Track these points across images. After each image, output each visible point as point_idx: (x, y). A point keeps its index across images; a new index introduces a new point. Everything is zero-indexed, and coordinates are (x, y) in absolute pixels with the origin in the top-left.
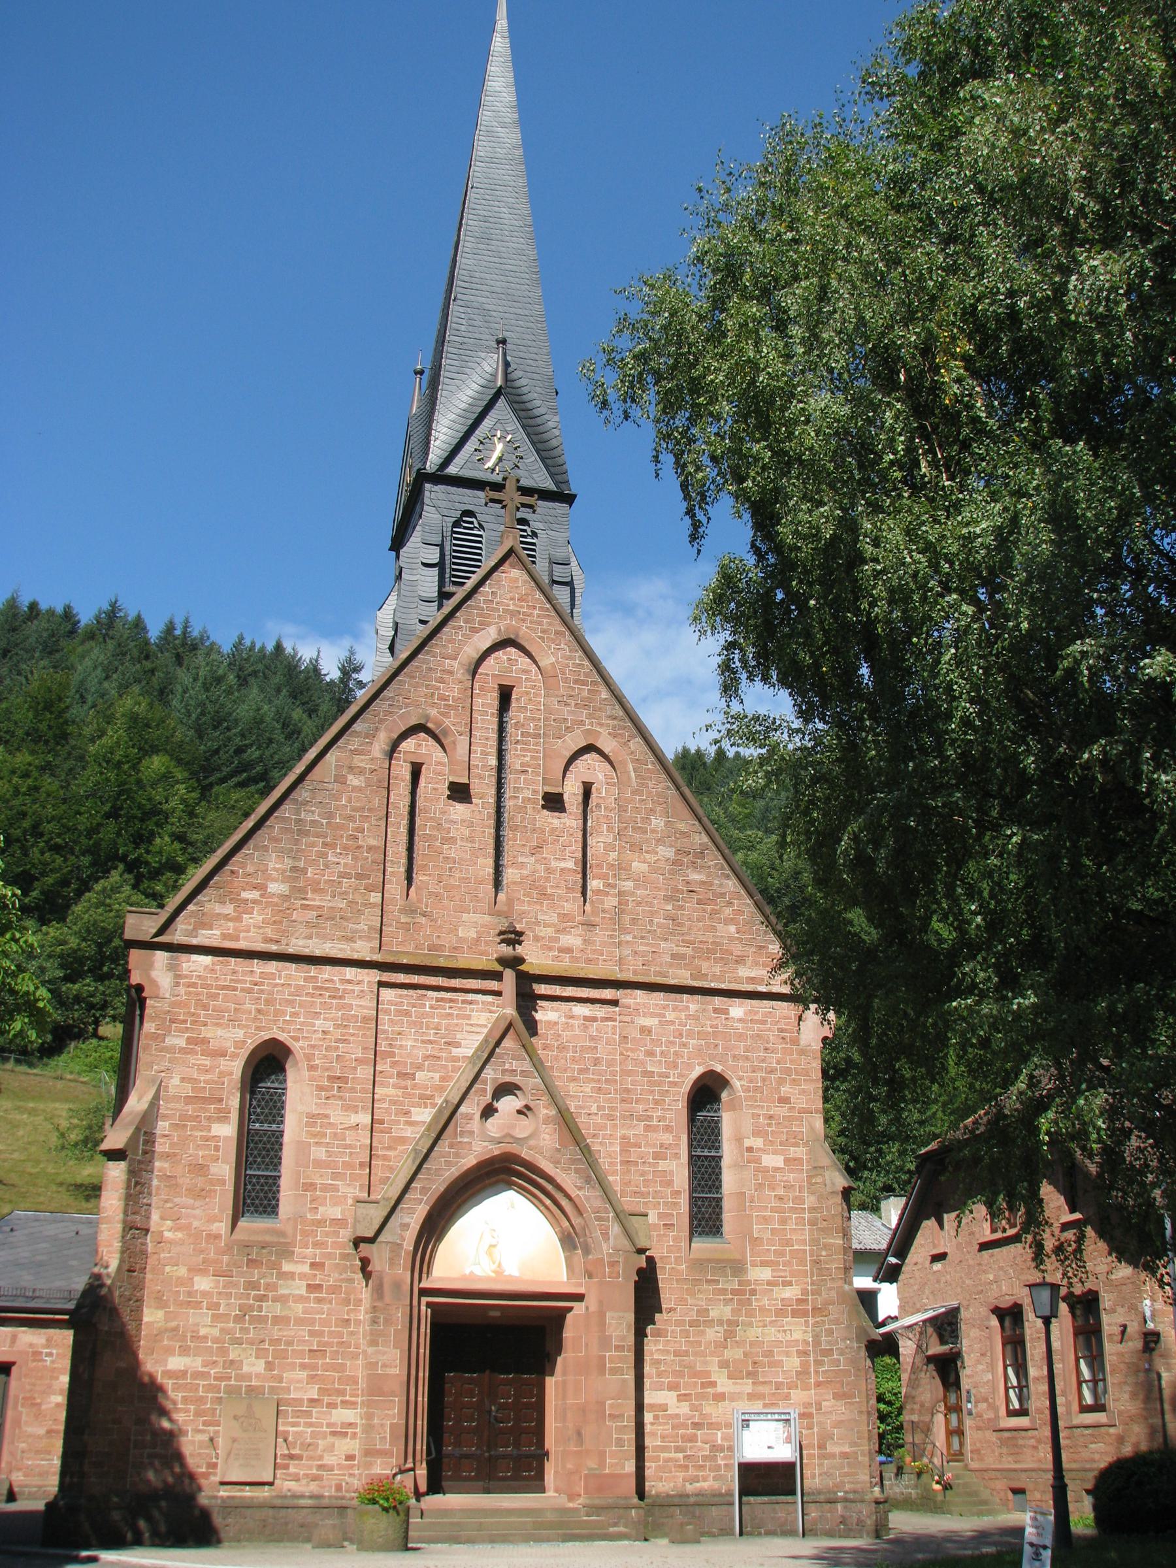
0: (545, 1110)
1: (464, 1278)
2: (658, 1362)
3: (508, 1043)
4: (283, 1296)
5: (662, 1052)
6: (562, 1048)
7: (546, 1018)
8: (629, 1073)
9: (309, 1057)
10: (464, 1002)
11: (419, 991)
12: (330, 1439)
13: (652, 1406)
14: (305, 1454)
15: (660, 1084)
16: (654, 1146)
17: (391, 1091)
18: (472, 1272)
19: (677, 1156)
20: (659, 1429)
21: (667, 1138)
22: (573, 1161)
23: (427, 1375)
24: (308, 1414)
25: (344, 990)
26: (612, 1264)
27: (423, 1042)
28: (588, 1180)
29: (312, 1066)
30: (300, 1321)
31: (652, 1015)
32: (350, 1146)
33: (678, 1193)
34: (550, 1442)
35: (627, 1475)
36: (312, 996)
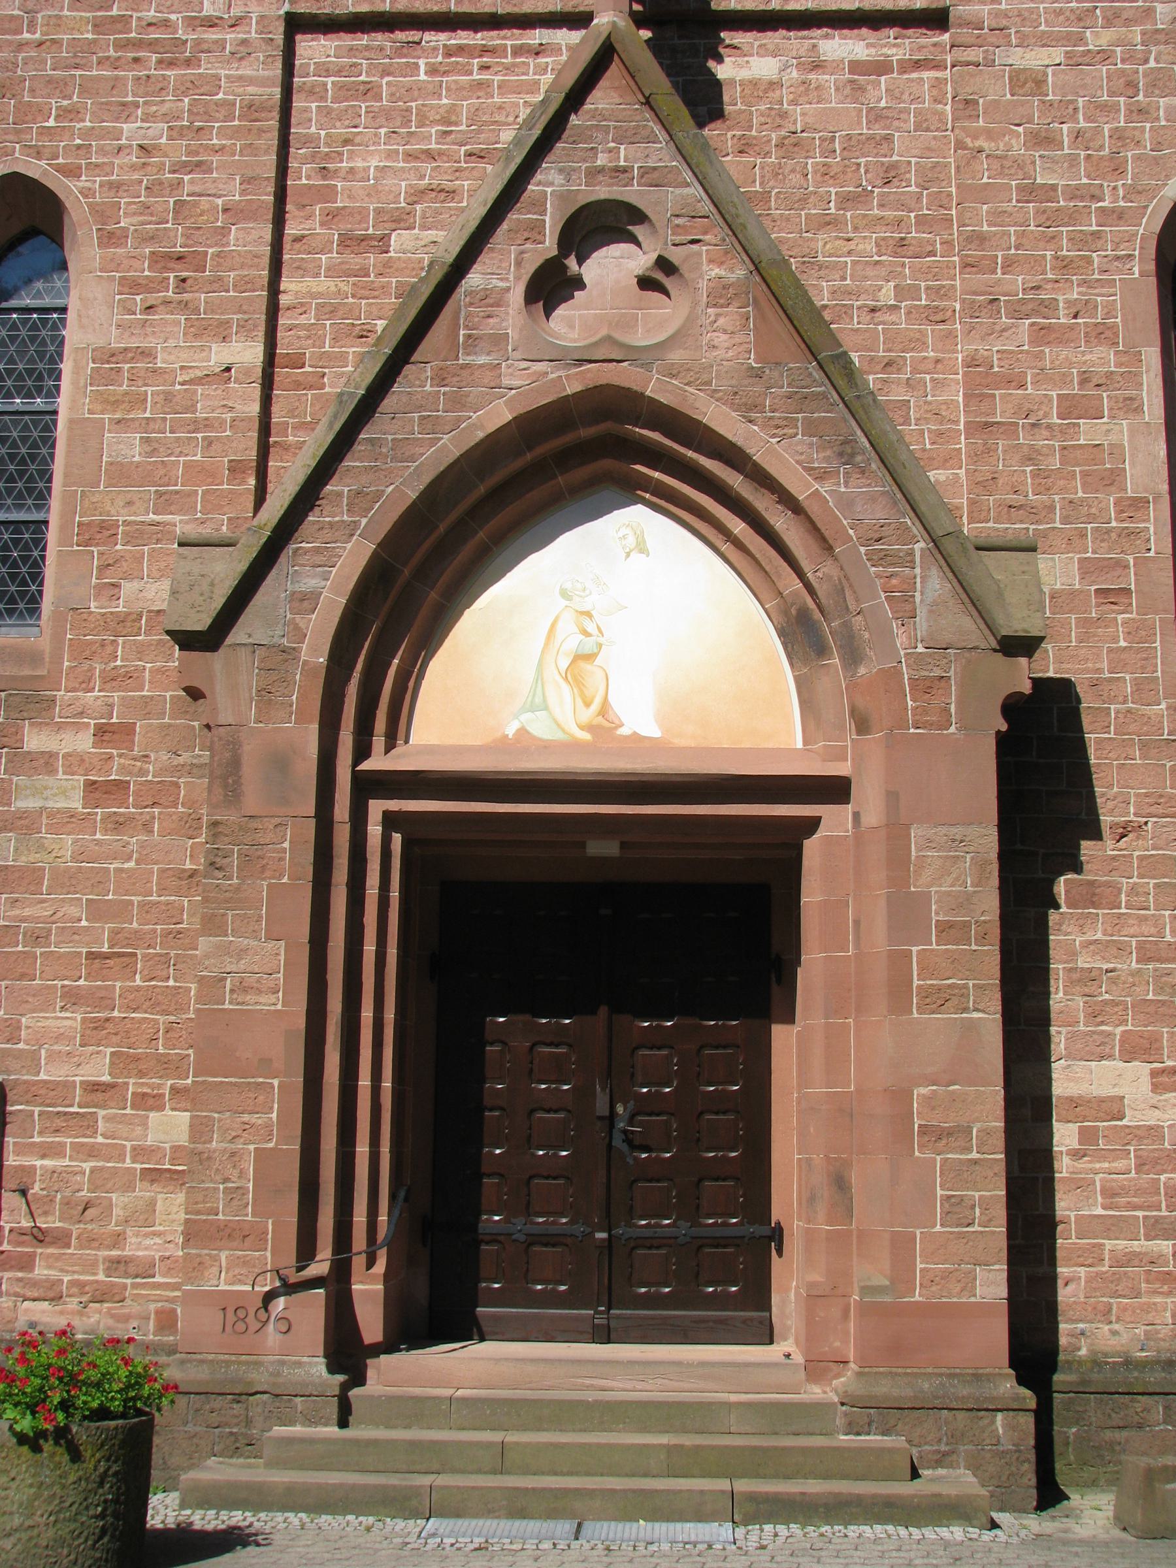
0: (711, 268)
1: (502, 745)
2: (1090, 978)
3: (601, 99)
4: (23, 815)
5: (1078, 135)
6: (793, 144)
7: (744, 74)
8: (983, 193)
9: (103, 214)
10: (518, 51)
11: (400, 36)
12: (143, 1192)
13: (1074, 1102)
14: (76, 1229)
15: (1072, 217)
16: (1065, 379)
17: (324, 284)
18: (522, 731)
19: (1131, 406)
20: (1100, 1170)
21: (1103, 359)
22: (802, 401)
23: (390, 1015)
24: (88, 1124)
25: (198, 42)
26: (926, 687)
27: (409, 156)
28: (846, 453)
29: (111, 234)
30: (66, 881)
31: (1046, 41)
32: (207, 424)
33: (1139, 503)
34: (786, 1203)
35: (983, 1309)
36: (115, 64)
